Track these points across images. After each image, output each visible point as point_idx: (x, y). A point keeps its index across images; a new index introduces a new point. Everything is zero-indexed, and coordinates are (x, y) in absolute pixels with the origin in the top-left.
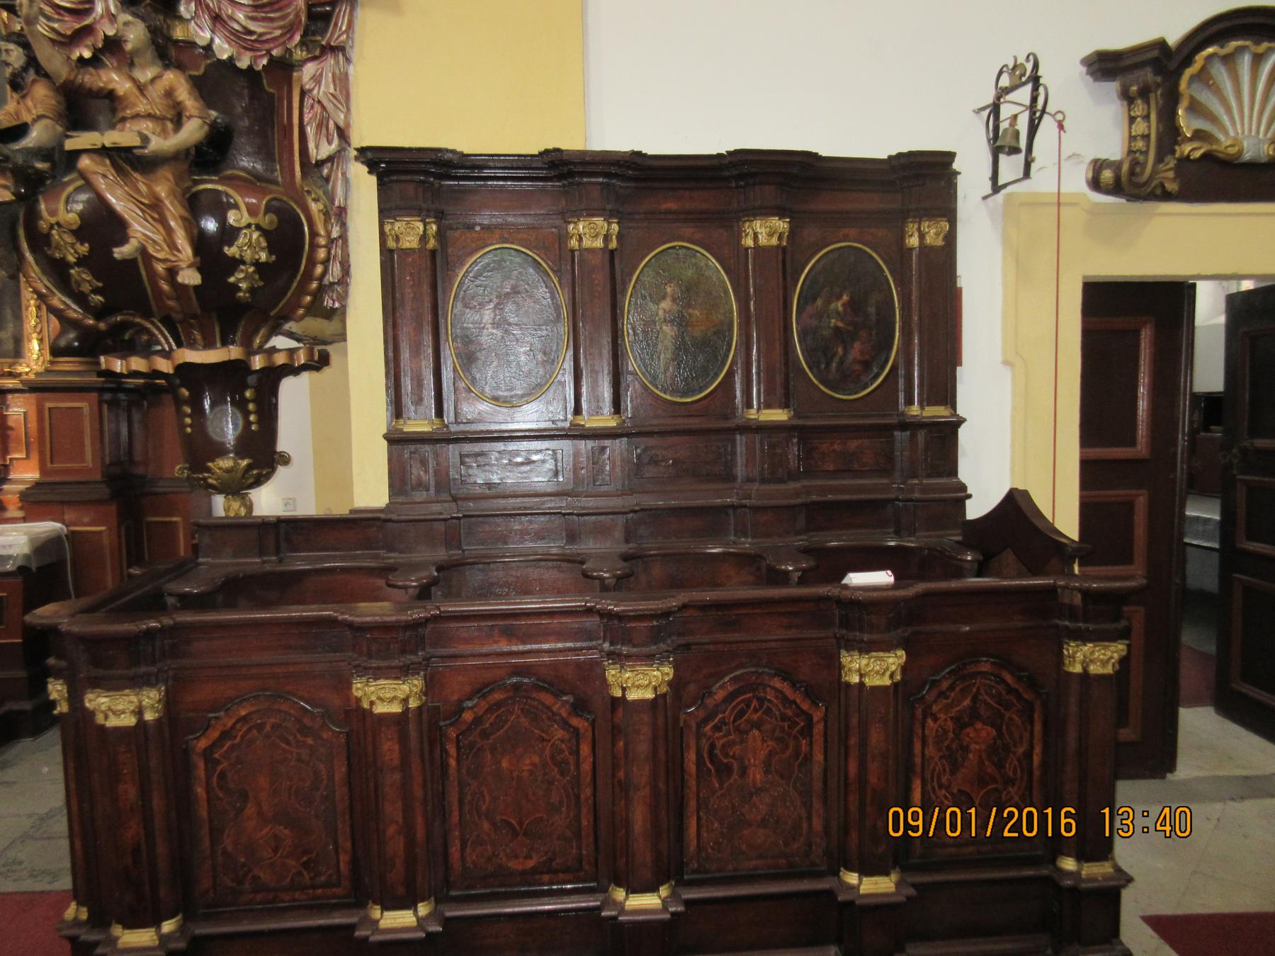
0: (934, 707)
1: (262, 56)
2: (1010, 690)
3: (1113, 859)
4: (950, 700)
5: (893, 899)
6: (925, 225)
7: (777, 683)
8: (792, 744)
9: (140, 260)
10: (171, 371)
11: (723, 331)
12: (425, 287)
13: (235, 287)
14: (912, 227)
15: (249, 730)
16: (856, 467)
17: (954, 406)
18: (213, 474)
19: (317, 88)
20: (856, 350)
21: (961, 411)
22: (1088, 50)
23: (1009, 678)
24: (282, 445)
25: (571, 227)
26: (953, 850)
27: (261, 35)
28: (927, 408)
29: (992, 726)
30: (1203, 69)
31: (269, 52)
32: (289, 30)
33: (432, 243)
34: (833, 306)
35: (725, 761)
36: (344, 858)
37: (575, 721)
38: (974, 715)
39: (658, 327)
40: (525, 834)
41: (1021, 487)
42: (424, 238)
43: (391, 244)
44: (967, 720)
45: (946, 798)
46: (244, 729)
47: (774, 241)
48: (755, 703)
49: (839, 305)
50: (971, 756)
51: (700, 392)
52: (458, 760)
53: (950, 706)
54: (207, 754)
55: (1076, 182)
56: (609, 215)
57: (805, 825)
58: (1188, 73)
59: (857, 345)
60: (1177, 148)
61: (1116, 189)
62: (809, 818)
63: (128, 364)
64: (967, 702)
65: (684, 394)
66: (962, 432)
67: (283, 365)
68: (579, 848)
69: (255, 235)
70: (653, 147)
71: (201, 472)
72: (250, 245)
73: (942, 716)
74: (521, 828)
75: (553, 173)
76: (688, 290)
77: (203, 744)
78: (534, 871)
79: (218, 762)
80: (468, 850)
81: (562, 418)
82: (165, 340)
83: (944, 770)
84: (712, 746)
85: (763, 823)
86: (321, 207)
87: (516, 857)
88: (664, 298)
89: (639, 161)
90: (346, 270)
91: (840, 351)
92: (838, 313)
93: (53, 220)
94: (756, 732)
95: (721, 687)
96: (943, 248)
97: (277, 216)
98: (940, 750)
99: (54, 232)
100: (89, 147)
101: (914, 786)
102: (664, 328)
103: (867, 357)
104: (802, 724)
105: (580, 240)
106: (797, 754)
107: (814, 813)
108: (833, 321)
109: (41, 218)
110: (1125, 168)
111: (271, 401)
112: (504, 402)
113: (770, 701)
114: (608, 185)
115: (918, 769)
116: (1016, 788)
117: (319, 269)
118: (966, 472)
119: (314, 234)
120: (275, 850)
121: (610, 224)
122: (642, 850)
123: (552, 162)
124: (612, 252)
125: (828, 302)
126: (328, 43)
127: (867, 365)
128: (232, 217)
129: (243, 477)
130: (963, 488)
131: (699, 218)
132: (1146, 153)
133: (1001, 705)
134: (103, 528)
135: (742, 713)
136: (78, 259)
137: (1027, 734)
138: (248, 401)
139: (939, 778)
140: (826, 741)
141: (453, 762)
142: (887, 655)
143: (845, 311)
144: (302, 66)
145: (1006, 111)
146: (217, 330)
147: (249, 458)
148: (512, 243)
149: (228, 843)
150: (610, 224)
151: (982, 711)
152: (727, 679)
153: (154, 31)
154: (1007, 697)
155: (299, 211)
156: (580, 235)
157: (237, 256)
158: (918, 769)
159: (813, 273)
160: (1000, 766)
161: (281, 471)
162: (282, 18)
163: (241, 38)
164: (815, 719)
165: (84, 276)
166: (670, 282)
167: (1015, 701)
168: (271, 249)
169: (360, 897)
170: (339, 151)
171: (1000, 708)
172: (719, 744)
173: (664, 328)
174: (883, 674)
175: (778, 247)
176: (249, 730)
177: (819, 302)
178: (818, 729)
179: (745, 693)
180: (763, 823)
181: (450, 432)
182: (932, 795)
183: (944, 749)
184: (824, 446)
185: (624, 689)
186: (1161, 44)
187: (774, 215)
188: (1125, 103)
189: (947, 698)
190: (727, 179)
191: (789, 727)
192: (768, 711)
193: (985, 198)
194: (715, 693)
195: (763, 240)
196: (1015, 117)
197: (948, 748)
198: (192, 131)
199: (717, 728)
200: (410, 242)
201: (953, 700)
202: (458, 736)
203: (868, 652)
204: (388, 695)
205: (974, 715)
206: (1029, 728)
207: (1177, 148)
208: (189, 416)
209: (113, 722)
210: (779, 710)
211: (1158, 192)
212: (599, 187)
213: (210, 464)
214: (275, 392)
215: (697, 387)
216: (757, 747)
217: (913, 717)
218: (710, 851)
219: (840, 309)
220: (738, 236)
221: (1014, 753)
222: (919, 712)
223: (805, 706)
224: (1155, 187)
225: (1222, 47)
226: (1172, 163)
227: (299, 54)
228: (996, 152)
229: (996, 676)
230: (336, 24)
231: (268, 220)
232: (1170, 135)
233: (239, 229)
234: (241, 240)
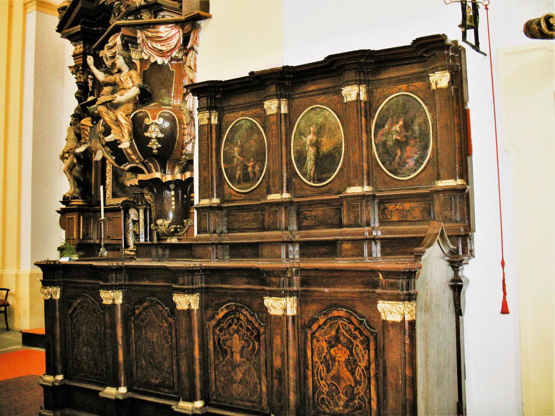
4: (325, 330)
8: (251, 343)
13: (151, 149)
29: (347, 348)
34: (394, 128)
38: (337, 339)
44: (334, 343)
48: (235, 320)
49: (397, 127)
53: (325, 333)
62: (260, 384)
64: (333, 333)
81: (391, 207)
83: (323, 370)
84: (219, 340)
91: (399, 152)
92: (397, 131)
94: (236, 335)
104: (255, 334)
106: (253, 349)
107: (262, 381)
108: (394, 136)
113: (241, 320)
125: (392, 125)
131: (325, 92)
133: (351, 336)
135: (230, 325)
137: (367, 355)
139: (321, 375)
149: (76, 351)
151: (341, 338)
152: (224, 307)
154: (354, 333)
167: (358, 335)
171: (351, 338)
172: (222, 339)
177: (386, 127)
179: (231, 315)
182: (318, 383)
183: (323, 358)
189: (323, 329)
197: (325, 357)
206: (367, 351)
216: (237, 343)
219: (398, 129)
222: (309, 336)
229: (348, 319)
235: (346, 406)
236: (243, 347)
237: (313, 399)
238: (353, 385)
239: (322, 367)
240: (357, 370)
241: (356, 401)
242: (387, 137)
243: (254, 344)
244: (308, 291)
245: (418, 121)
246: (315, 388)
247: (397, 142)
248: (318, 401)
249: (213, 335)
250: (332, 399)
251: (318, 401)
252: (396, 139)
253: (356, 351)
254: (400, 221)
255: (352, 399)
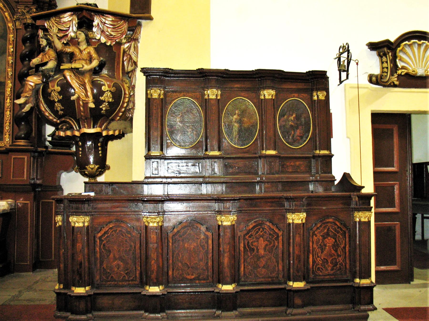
0: (316, 232)
1: (114, 42)
2: (338, 227)
3: (371, 279)
4: (320, 230)
5: (303, 288)
6: (319, 93)
7: (268, 224)
9: (76, 100)
10: (79, 136)
11: (254, 126)
12: (160, 110)
13: (102, 109)
14: (315, 94)
15: (112, 231)
16: (299, 171)
17: (330, 151)
18: (87, 170)
19: (128, 51)
20: (298, 132)
21: (333, 153)
22: (367, 42)
23: (338, 224)
24: (108, 163)
25: (206, 92)
26: (323, 277)
27: (114, 36)
28: (321, 151)
29: (333, 238)
30: (403, 48)
31: (116, 40)
32: (122, 34)
33: (162, 97)
34: (290, 118)
35: (252, 247)
36: (138, 273)
37: (207, 233)
38: (328, 234)
39: (233, 124)
40: (191, 268)
41: (347, 172)
42: (159, 95)
43: (149, 96)
45: (320, 261)
46: (111, 231)
47: (270, 97)
49: (292, 118)
50: (327, 247)
51: (247, 145)
52: (172, 244)
54: (100, 238)
55: (365, 81)
56: (217, 88)
57: (277, 268)
58: (399, 49)
59: (298, 130)
60: (397, 71)
61: (377, 83)
62: (278, 266)
63: (65, 134)
64: (326, 231)
65: (242, 146)
66: (333, 159)
67: (112, 135)
68: (208, 272)
69: (109, 93)
70: (231, 68)
71: (83, 169)
72: (107, 96)
73: (318, 235)
74: (190, 265)
75: (200, 76)
76: (243, 112)
77: (100, 235)
78: (194, 279)
79: (103, 241)
80: (174, 272)
82: (75, 126)
83: (319, 252)
84: (248, 243)
85: (264, 267)
86: (128, 85)
87: (189, 275)
88: (235, 114)
89: (228, 72)
90: (134, 106)
92: (292, 120)
93: (53, 89)
94: (262, 238)
95: (252, 224)
96: (324, 100)
97: (116, 88)
98: (317, 246)
99: (52, 92)
100: (68, 68)
101: (310, 257)
102: (235, 124)
103: (302, 135)
104: (276, 236)
105: (209, 96)
106: (274, 246)
109: (49, 88)
110: (379, 77)
111: (105, 147)
112: (183, 147)
113: (266, 229)
114: (217, 79)
115: (311, 251)
116: (341, 258)
117: (125, 105)
118: (334, 173)
119: (125, 94)
120: (118, 269)
121: (218, 91)
122: (227, 271)
123: (200, 72)
124: (219, 100)
125: (288, 117)
126: (133, 38)
127: (302, 137)
128: (103, 88)
129: (96, 171)
130: (334, 177)
131: (247, 90)
132: (387, 73)
133: (336, 232)
134: (28, 202)
135: (257, 232)
136: (58, 100)
138: (99, 147)
139: (318, 255)
140: (283, 242)
141: (171, 244)
142: (300, 214)
143: (294, 120)
144: (125, 44)
145: (342, 59)
146: (92, 123)
147: (99, 165)
148: (187, 97)
149: (105, 266)
150: (218, 91)
151: (330, 234)
152: (253, 222)
153: (87, 36)
155: (121, 86)
156: (208, 95)
157: (103, 100)
158: (311, 251)
159: (283, 108)
160: (336, 251)
161: (107, 171)
162: (121, 31)
163: (109, 37)
164: (280, 235)
165: (59, 105)
166: (237, 110)
168: (113, 98)
169: (144, 283)
170: (134, 69)
172: (250, 242)
173: (235, 124)
174: (299, 219)
175: (272, 99)
176: (112, 231)
177: (286, 117)
178: (281, 238)
179: (258, 226)
180: (264, 267)
181: (165, 156)
184: (288, 163)
185: (222, 222)
186: (388, 41)
187: (271, 89)
188: (380, 57)
189: (320, 229)
190: (255, 78)
191: (272, 237)
192: (265, 232)
193: (339, 85)
194: (249, 226)
195: (267, 97)
196: (344, 61)
197: (320, 245)
198: (95, 63)
199: (249, 237)
200: (155, 96)
201: (321, 230)
202: (172, 236)
203: (294, 213)
204: (153, 221)
205: (328, 234)
206: (345, 239)
207: (397, 71)
208: (81, 151)
209: (77, 225)
210: (269, 232)
211: (392, 84)
212: (214, 80)
213: (87, 167)
214: (106, 145)
215: (246, 143)
216: (262, 243)
217: (309, 235)
218: (248, 275)
219: (292, 119)
220: (259, 95)
221: (340, 247)
222: (311, 234)
223: (277, 231)
224: (391, 83)
225: (409, 42)
226: (396, 75)
227: (124, 41)
228: (340, 71)
229: (334, 223)
230: (136, 32)
231: (113, 89)
232: (395, 67)
233: (105, 92)
234: (105, 95)
235: (332, 269)
236: (266, 245)
237: (313, 268)
238: (336, 258)
239: (319, 250)
240: (339, 249)
241: (338, 266)
242: (286, 123)
243: (274, 243)
244: (311, 209)
245: (304, 115)
246: (314, 262)
247: (291, 126)
248: (315, 270)
249: (244, 240)
250: (324, 267)
251: (315, 270)
252: (291, 125)
253: (338, 239)
254: (293, 172)
255: (336, 265)
